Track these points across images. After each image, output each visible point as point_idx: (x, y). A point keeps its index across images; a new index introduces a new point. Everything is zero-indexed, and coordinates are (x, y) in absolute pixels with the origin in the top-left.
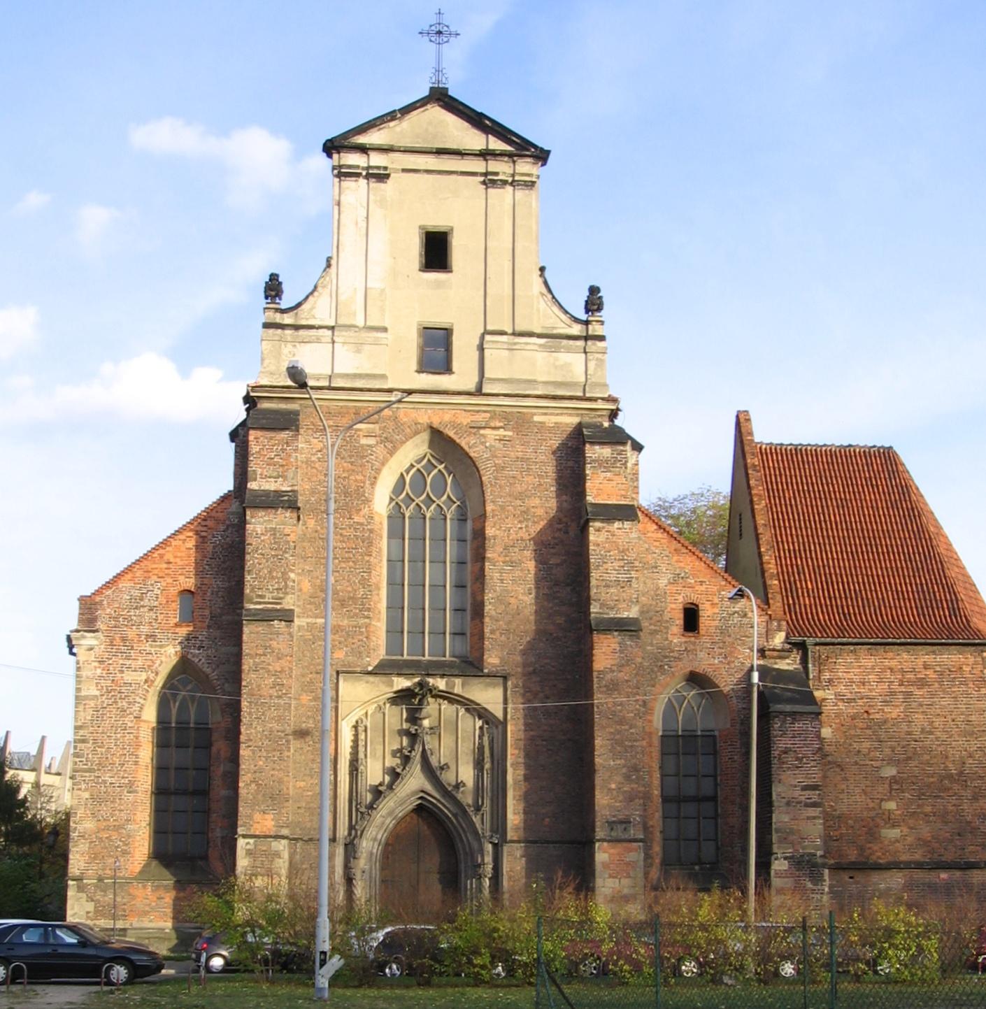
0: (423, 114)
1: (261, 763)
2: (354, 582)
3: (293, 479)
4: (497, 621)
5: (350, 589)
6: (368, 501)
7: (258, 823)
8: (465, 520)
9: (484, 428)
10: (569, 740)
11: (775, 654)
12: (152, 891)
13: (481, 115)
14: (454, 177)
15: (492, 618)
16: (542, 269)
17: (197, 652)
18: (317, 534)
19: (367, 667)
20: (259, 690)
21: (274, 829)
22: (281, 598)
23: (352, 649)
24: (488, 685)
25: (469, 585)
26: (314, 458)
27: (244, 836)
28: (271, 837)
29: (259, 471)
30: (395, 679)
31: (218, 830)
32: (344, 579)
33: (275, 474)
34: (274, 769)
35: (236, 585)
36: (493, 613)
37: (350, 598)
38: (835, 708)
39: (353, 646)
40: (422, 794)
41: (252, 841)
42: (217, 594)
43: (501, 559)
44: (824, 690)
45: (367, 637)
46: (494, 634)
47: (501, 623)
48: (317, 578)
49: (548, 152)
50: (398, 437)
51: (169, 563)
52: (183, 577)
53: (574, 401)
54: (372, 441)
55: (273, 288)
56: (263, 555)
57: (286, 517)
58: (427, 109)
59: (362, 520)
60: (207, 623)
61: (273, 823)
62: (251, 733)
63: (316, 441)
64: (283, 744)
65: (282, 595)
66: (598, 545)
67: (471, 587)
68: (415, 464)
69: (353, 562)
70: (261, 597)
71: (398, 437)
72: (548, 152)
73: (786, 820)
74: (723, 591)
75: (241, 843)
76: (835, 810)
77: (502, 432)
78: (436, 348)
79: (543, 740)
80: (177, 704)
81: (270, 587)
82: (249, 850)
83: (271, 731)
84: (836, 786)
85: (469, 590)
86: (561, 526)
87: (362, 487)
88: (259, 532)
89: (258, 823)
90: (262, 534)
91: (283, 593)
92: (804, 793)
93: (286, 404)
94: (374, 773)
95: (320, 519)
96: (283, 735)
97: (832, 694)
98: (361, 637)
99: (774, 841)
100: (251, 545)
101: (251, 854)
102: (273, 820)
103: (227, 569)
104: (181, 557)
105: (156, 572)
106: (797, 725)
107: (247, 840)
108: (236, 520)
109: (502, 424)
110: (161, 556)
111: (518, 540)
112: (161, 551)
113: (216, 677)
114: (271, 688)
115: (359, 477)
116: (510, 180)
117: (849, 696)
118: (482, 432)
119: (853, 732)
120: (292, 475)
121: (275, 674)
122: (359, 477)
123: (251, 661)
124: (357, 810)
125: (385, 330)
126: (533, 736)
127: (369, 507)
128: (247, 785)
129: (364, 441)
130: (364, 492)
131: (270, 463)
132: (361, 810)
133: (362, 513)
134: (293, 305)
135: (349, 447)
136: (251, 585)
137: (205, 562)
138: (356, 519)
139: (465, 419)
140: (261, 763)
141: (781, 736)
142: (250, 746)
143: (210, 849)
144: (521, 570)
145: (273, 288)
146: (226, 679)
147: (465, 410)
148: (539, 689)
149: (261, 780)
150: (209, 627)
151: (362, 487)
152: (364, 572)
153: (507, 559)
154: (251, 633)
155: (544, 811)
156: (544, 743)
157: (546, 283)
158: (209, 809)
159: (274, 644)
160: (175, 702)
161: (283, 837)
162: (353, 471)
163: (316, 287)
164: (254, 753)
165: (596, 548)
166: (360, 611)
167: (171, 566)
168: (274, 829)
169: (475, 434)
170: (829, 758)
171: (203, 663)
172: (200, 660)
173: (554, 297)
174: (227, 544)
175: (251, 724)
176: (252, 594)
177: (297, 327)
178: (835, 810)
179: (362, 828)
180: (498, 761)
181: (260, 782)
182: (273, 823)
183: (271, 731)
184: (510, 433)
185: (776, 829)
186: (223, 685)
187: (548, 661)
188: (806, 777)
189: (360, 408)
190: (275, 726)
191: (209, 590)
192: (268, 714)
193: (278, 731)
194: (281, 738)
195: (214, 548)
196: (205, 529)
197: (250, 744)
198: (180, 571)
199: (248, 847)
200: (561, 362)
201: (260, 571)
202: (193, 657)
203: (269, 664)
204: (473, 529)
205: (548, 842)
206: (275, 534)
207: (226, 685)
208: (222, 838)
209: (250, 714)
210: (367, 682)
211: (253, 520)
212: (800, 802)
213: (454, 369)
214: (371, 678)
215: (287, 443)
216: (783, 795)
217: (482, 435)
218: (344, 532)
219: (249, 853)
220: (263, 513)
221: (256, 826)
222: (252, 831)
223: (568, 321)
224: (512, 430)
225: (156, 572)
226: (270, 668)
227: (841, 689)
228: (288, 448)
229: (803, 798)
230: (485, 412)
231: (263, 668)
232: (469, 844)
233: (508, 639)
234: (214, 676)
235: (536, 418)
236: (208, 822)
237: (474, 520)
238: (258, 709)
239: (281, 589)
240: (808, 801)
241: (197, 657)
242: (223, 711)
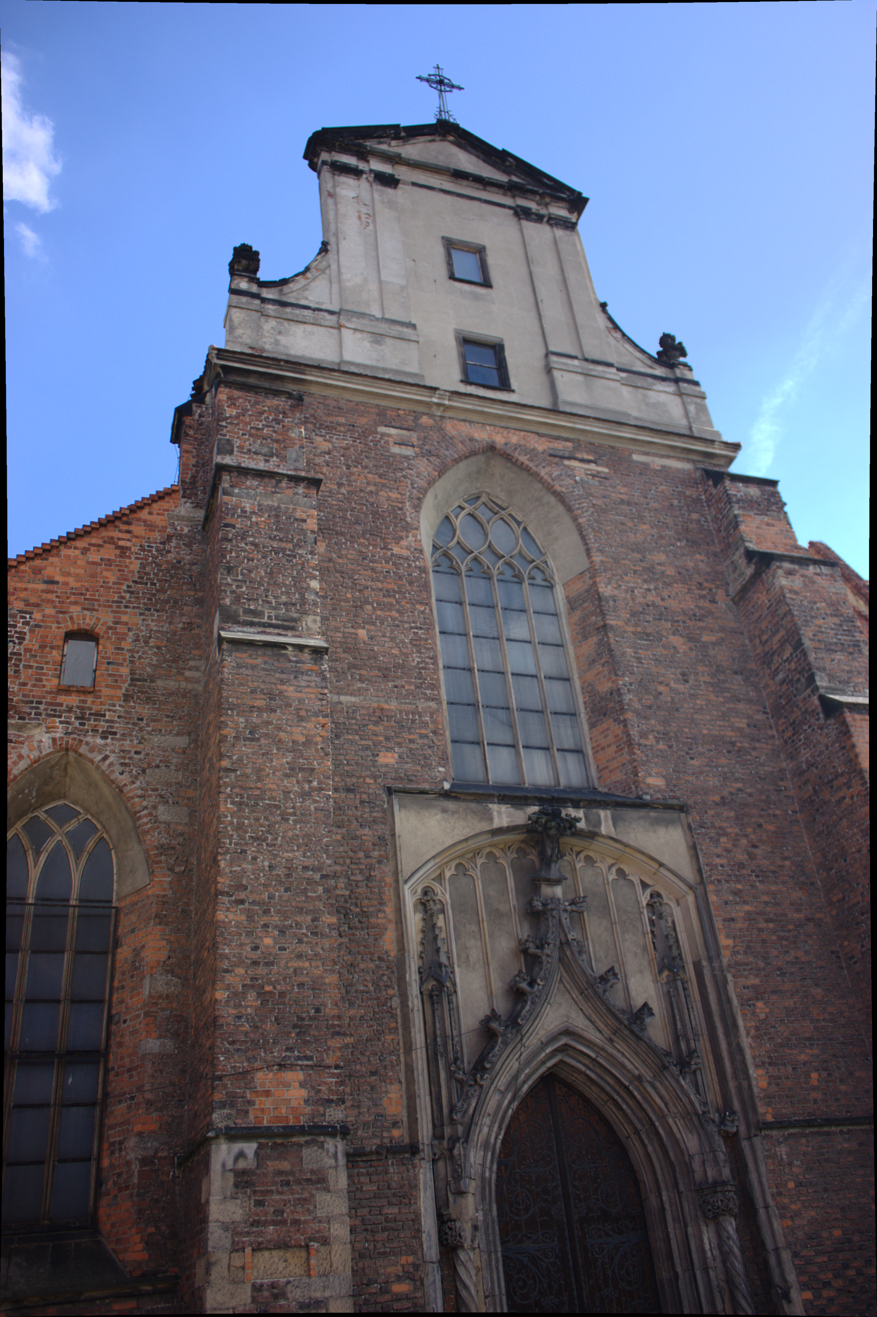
0: (429, 145)
1: (268, 941)
2: (403, 642)
3: (296, 461)
4: (645, 718)
5: (395, 651)
6: (410, 528)
7: (267, 1093)
8: (551, 587)
9: (569, 458)
10: (808, 920)
12: (325, 1006)
13: (505, 154)
14: (476, 204)
15: (637, 712)
16: (603, 306)
17: (99, 741)
18: (332, 565)
19: (441, 781)
20: (259, 779)
21: (308, 1109)
22: (294, 620)
23: (411, 750)
24: (656, 822)
25: (576, 677)
26: (318, 460)
27: (233, 1135)
28: (301, 1130)
29: (237, 443)
30: (494, 807)
31: (132, 1142)
32: (384, 636)
33: (265, 450)
34: (300, 956)
35: (184, 629)
36: (637, 706)
37: (397, 666)
39: (411, 746)
40: (564, 1040)
41: (250, 1148)
42: (146, 642)
43: (631, 629)
45: (435, 732)
46: (647, 738)
47: (653, 722)
48: (337, 629)
49: (586, 200)
50: (447, 453)
51: (53, 582)
52: (78, 608)
54: (409, 452)
55: (245, 260)
56: (256, 545)
57: (297, 494)
58: (433, 141)
59: (405, 553)
60: (123, 691)
61: (304, 1093)
62: (244, 871)
63: (320, 439)
64: (319, 898)
65: (295, 615)
66: (796, 593)
67: (580, 677)
68: (465, 505)
69: (398, 611)
70: (254, 613)
71: (447, 453)
72: (586, 200)
75: (223, 1154)
77: (592, 466)
78: (485, 361)
79: (767, 921)
80: (43, 858)
81: (271, 598)
82: (244, 1172)
83: (290, 869)
85: (577, 684)
86: (704, 592)
87: (400, 509)
88: (248, 509)
89: (267, 1093)
90: (254, 513)
91: (297, 611)
94: (475, 992)
95: (336, 544)
96: (317, 877)
98: (423, 731)
100: (234, 527)
101: (248, 1184)
102: (302, 1085)
103: (168, 601)
104: (77, 575)
105: (23, 595)
107: (237, 1146)
108: (186, 530)
109: (591, 458)
110: (37, 571)
111: (648, 605)
112: (38, 562)
113: (140, 792)
114: (287, 776)
115: (394, 495)
116: (222, 773)
118: (566, 462)
120: (294, 455)
121: (295, 748)
122: (394, 495)
123: (242, 720)
124: (451, 1075)
126: (748, 913)
127: (415, 536)
128: (236, 994)
129: (396, 450)
130: (405, 514)
131: (256, 433)
132: (463, 1070)
133: (404, 543)
134: (277, 278)
135: (373, 455)
136: (232, 592)
137: (125, 587)
138: (396, 550)
139: (541, 446)
140: (268, 941)
142: (242, 902)
143: (104, 1202)
144: (664, 647)
145: (245, 260)
146: (161, 796)
147: (538, 434)
148: (737, 830)
149: (269, 983)
150: (127, 697)
151: (400, 509)
152: (416, 628)
153: (639, 629)
154: (239, 666)
155: (803, 1057)
156: (771, 925)
157: (610, 319)
158: (106, 1094)
159: (290, 691)
160: (38, 854)
161: (331, 1131)
162: (384, 485)
163: (307, 269)
164: (250, 918)
165: (794, 597)
166: (417, 687)
167: (55, 587)
168: (308, 1109)
169: (556, 464)
171: (111, 764)
172: (106, 758)
173: (624, 335)
174: (167, 562)
175: (244, 852)
176: (234, 607)
177: (283, 304)
179: (467, 1119)
180: (698, 966)
181: (268, 988)
182: (304, 1093)
183: (290, 869)
184: (606, 470)
186: (155, 807)
187: (740, 785)
189: (386, 408)
190: (297, 856)
191: (131, 634)
192: (281, 828)
193: (306, 868)
194: (310, 881)
195: (143, 566)
196: (128, 536)
197: (242, 895)
198: (73, 598)
199: (242, 1165)
200: (653, 400)
201: (250, 571)
202: (92, 750)
203: (280, 729)
204: (567, 597)
205: (829, 1122)
206: (277, 516)
207: (161, 808)
208: (144, 1161)
209: (240, 827)
210: (444, 811)
211: (236, 491)
213: (513, 387)
214: (450, 805)
215: (284, 413)
217: (568, 467)
218: (378, 566)
219: (243, 1180)
220: (255, 483)
221: (261, 1102)
222: (251, 1117)
223: (649, 362)
224: (607, 466)
225: (23, 595)
226: (282, 735)
228: (286, 420)
230: (567, 440)
231: (267, 736)
232: (676, 1142)
233: (670, 747)
234: (134, 789)
235: (635, 457)
236: (102, 1125)
237: (565, 585)
238: (257, 819)
239: (294, 605)
241: (100, 751)
242: (151, 864)
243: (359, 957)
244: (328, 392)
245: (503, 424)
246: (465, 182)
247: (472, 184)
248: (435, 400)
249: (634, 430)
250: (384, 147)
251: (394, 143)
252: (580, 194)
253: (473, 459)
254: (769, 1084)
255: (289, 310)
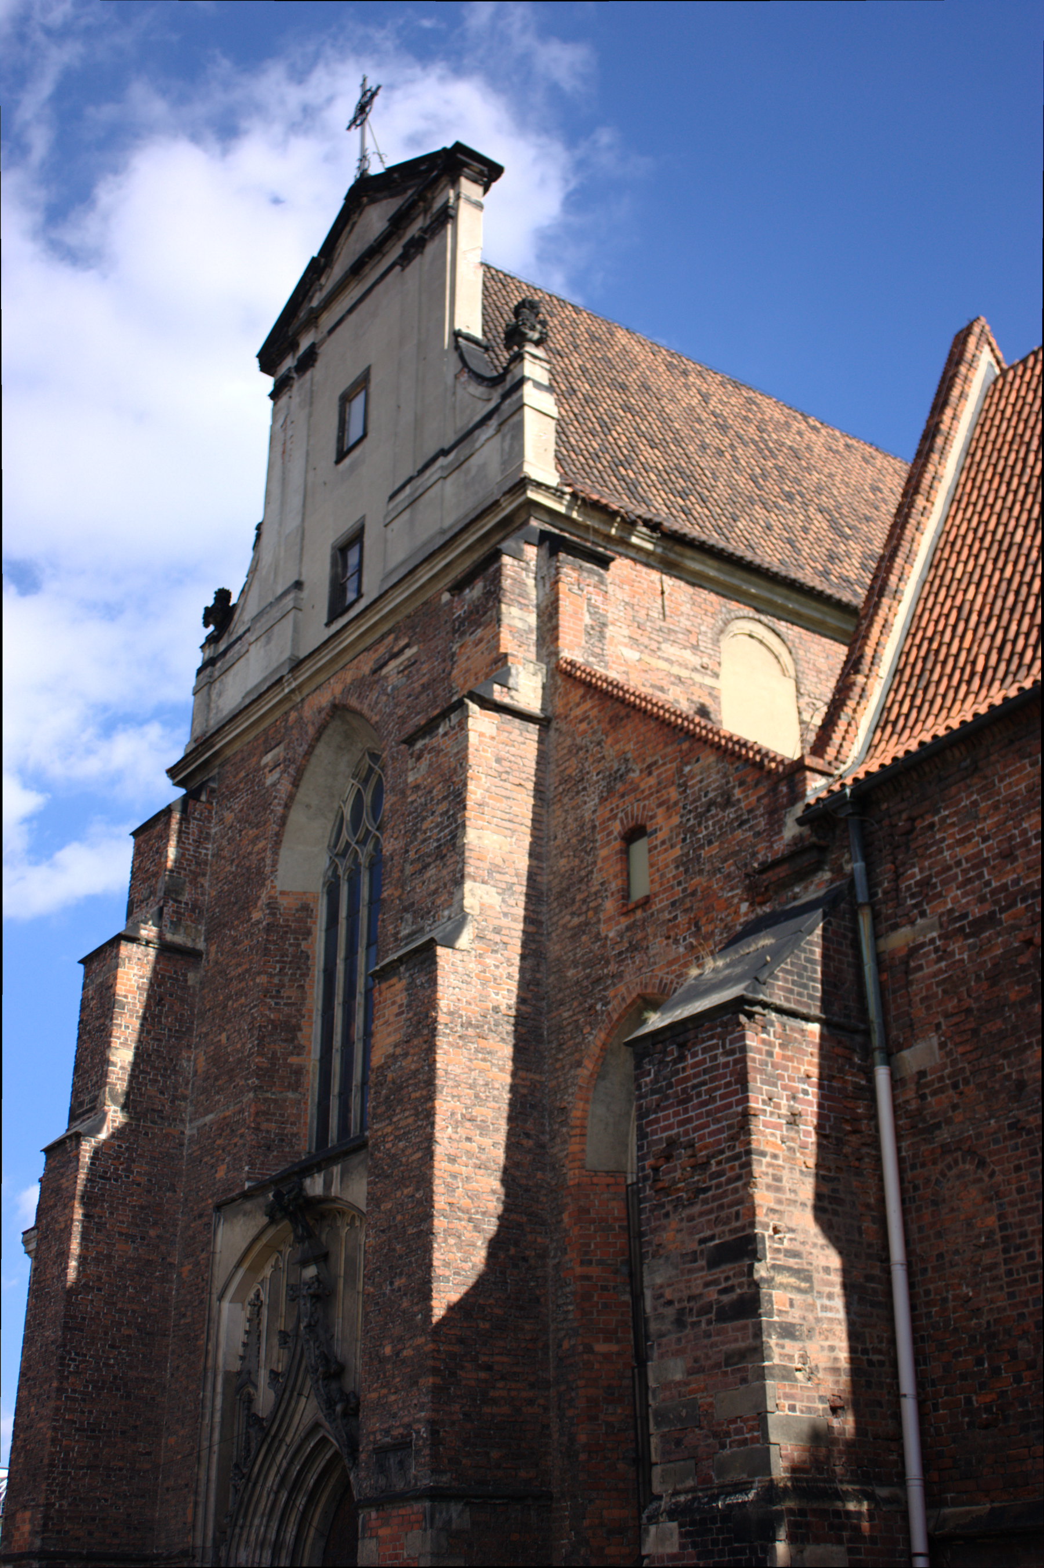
11: (782, 871)
38: (943, 964)
44: (912, 923)
53: (473, 529)
58: (354, 224)
73: (678, 1377)
74: (687, 763)
76: (977, 1312)
84: (970, 1225)
92: (718, 1273)
93: (909, 559)
97: (931, 928)
99: (654, 1458)
106: (690, 1061)
117: (976, 912)
119: (996, 1025)
125: (356, 538)
141: (658, 1108)
170: (944, 1135)
178: (977, 1312)
185: (656, 1413)
188: (717, 1221)
212: (706, 1310)
216: (668, 1294)
227: (954, 898)
229: (712, 1294)
240: (725, 1298)
243: (570, 1413)
244: (237, 746)
245: (341, 664)
246: (367, 269)
247: (373, 262)
248: (287, 690)
249: (426, 567)
250: (315, 303)
251: (323, 281)
252: (444, 149)
253: (329, 732)
254: (682, 1546)
255: (228, 656)
